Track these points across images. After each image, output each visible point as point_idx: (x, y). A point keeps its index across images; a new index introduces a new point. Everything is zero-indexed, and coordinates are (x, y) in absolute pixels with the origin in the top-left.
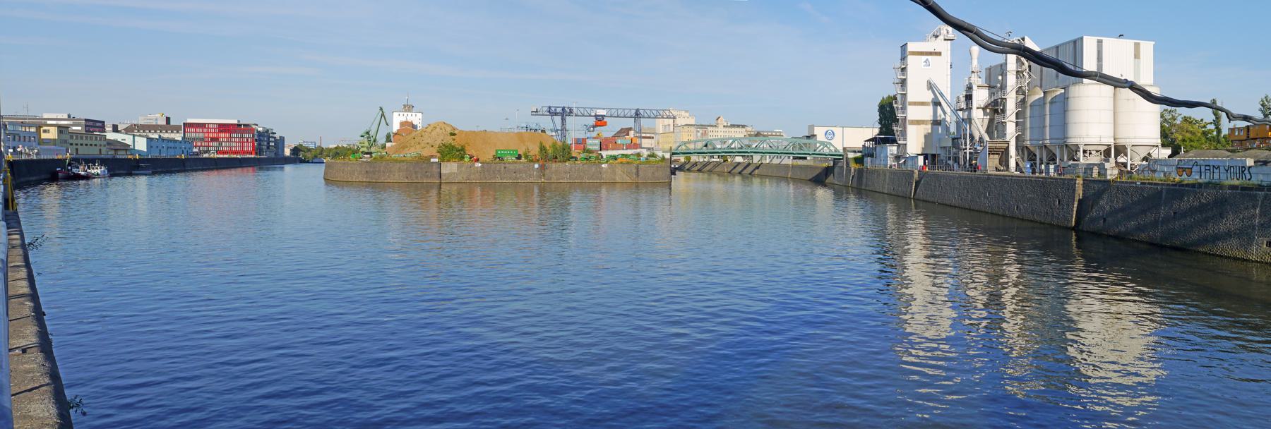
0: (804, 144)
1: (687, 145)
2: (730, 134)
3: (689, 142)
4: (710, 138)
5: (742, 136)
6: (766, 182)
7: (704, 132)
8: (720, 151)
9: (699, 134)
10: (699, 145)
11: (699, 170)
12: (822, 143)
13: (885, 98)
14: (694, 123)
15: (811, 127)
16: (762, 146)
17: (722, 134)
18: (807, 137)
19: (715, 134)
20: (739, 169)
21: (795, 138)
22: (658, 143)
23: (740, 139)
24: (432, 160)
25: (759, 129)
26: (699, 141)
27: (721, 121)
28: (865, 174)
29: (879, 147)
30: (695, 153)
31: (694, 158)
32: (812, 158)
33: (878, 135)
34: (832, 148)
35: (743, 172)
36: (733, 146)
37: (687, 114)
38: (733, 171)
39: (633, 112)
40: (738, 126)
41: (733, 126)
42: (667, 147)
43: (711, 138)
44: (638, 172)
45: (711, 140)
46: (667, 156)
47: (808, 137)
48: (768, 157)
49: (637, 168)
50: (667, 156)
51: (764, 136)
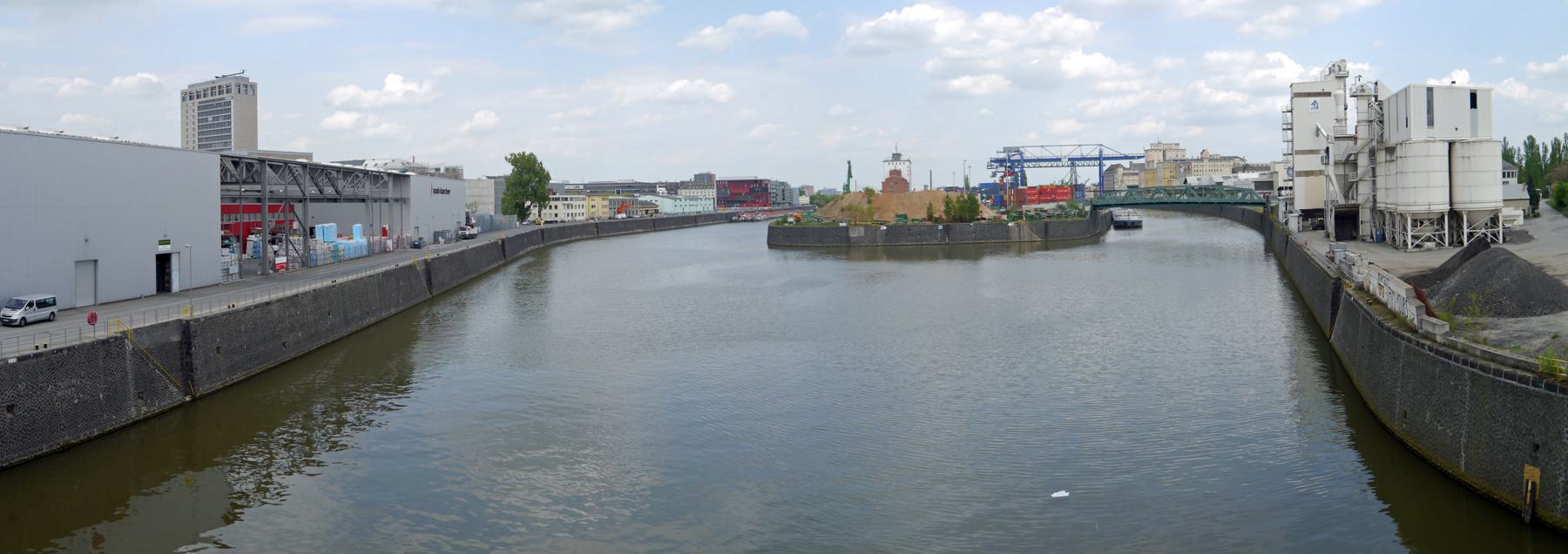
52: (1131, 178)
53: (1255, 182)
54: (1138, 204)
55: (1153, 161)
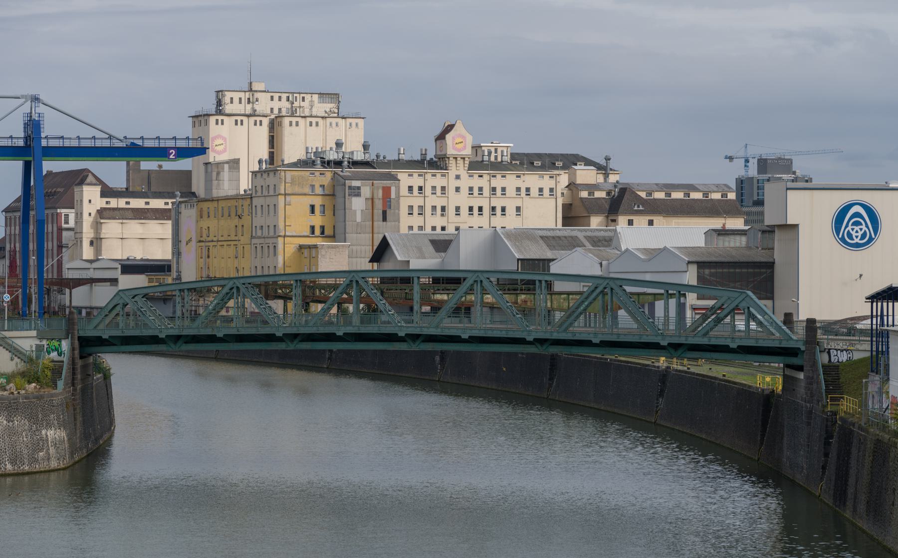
52: (135, 227)
53: (701, 265)
54: (154, 340)
55: (234, 164)
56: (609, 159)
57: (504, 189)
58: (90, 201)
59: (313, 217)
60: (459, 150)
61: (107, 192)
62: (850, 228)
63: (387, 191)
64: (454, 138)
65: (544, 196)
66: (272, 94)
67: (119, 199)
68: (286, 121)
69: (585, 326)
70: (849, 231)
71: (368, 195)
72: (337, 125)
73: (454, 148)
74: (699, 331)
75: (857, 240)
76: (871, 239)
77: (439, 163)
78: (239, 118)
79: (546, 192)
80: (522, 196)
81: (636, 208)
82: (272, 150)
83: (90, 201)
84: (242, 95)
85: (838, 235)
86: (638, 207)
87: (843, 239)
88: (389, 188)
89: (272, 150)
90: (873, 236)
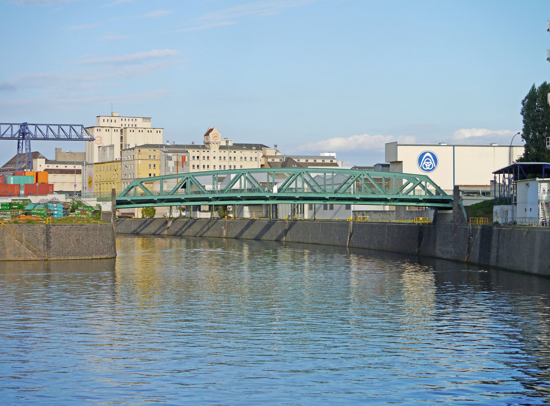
0: (375, 180)
1: (146, 186)
2: (232, 163)
3: (152, 179)
4: (192, 170)
5: (256, 165)
6: (303, 254)
7: (180, 160)
8: (211, 196)
9: (171, 164)
10: (170, 186)
11: (177, 235)
12: (412, 178)
13: (537, 87)
14: (161, 142)
15: (392, 147)
16: (293, 186)
17: (217, 162)
18: (383, 165)
19: (202, 162)
20: (254, 231)
21: (360, 168)
22: (90, 182)
23: (250, 171)
24: (255, 148)
25: (289, 153)
26: (171, 177)
27: (216, 137)
28: (494, 238)
29: (521, 185)
30: (162, 200)
31: (161, 211)
32: (394, 208)
33: (521, 160)
34: (431, 188)
35: (264, 238)
36: (237, 186)
37: (148, 125)
38: (205, 235)
39: (16, 129)
40: (249, 147)
41: (238, 147)
42: (107, 190)
43: (196, 170)
44: (48, 238)
45: (194, 175)
46: (107, 207)
47: (385, 166)
48: (306, 207)
49: (47, 231)
50: (107, 207)
51: (300, 165)
56: (276, 146)
57: (235, 158)
58: (40, 165)
59: (150, 170)
60: (215, 140)
61: (47, 162)
62: (425, 163)
63: (184, 158)
64: (213, 135)
65: (253, 161)
66: (122, 118)
67: (54, 165)
68: (128, 130)
69: (303, 204)
70: (424, 164)
71: (176, 160)
72: (133, 131)
73: (213, 139)
74: (181, 309)
75: (428, 168)
76: (434, 168)
77: (205, 146)
78: (107, 129)
79: (254, 159)
80: (243, 160)
81: (293, 166)
82: (121, 143)
83: (40, 165)
84: (108, 118)
85: (420, 166)
86: (295, 166)
87: (422, 168)
88: (185, 157)
89: (121, 143)
90: (435, 166)
